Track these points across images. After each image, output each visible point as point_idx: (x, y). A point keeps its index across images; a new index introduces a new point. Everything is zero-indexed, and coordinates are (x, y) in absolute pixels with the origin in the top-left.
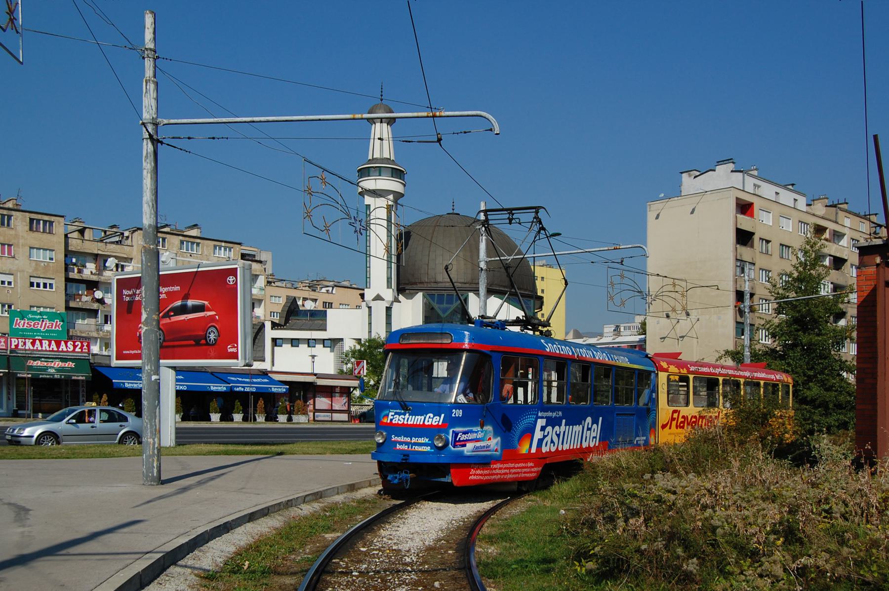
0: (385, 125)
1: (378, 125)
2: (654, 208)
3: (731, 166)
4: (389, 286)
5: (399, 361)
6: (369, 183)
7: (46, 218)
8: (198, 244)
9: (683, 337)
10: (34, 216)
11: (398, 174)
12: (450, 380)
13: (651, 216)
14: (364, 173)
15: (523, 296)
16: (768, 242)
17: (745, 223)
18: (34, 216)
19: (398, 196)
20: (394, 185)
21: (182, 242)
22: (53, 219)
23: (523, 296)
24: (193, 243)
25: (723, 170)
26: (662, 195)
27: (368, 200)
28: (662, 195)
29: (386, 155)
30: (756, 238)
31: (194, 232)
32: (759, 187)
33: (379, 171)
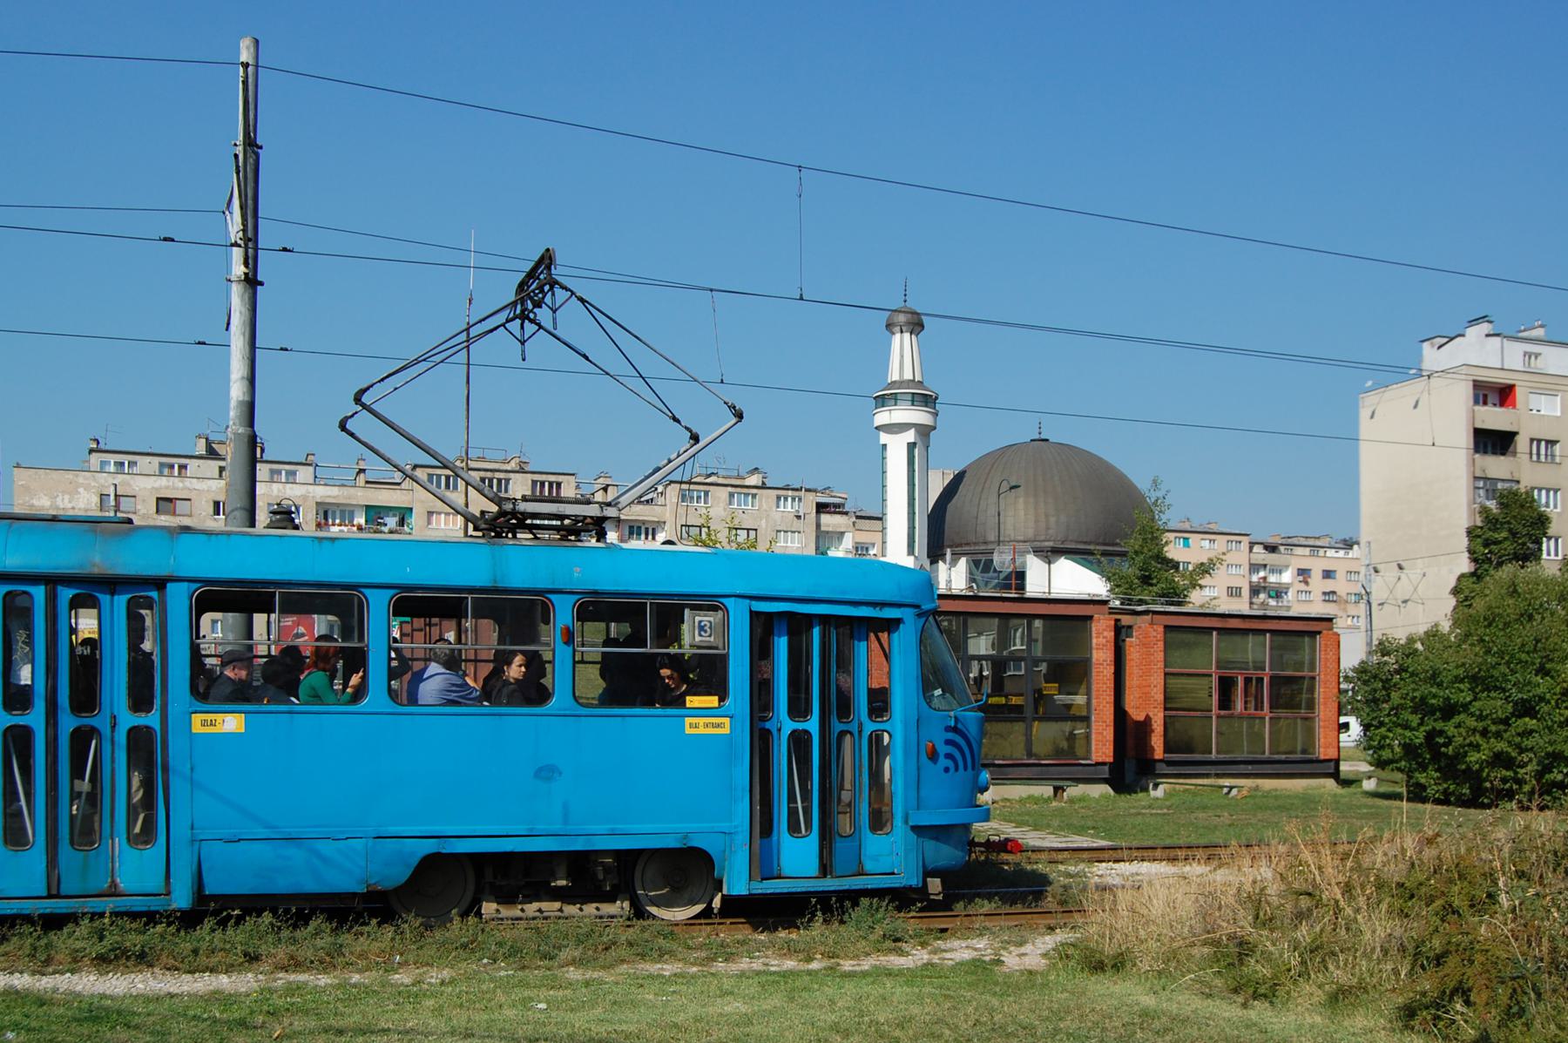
0: (907, 336)
1: (898, 336)
2: (1368, 402)
3: (1485, 328)
4: (911, 551)
5: (459, 625)
6: (883, 417)
7: (553, 478)
8: (754, 496)
9: (1405, 602)
10: (536, 477)
11: (927, 401)
12: (608, 642)
13: (1364, 414)
14: (882, 401)
15: (1104, 554)
16: (1551, 443)
17: (1495, 418)
18: (536, 477)
19: (924, 431)
20: (920, 416)
21: (731, 495)
22: (560, 479)
23: (1104, 554)
24: (747, 495)
25: (1476, 332)
26: (1370, 383)
27: (884, 438)
28: (1370, 383)
29: (908, 376)
30: (1522, 443)
31: (754, 480)
32: (1537, 355)
33: (895, 399)
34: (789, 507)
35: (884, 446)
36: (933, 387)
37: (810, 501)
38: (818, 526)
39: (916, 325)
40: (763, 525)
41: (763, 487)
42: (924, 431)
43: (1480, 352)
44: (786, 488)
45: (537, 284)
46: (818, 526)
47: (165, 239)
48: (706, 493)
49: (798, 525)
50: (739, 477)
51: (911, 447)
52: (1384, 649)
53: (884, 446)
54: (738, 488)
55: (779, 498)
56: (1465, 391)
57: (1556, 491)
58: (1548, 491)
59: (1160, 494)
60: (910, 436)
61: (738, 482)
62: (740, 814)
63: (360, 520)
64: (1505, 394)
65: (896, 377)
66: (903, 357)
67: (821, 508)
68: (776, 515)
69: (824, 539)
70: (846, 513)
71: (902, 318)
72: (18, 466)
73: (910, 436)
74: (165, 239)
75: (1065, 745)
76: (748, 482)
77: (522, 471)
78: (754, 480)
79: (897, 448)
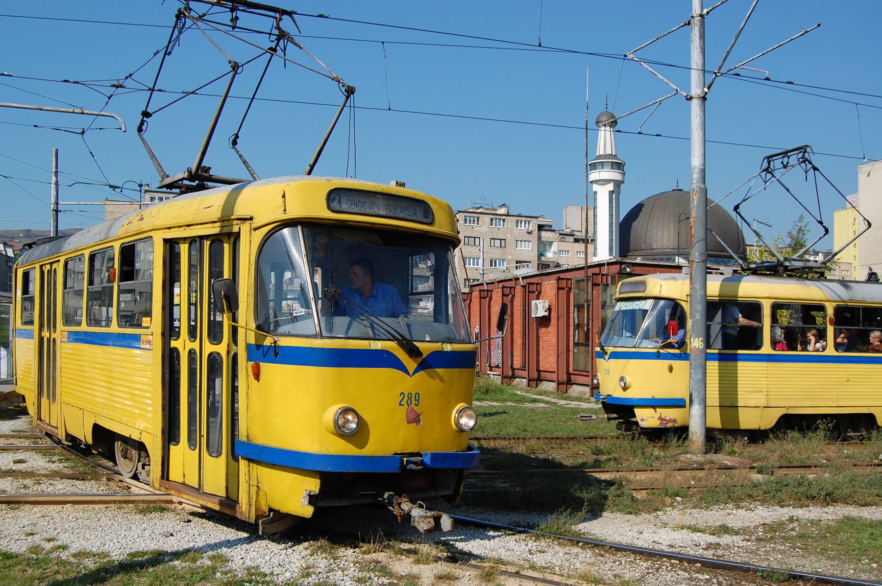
0: (608, 128)
4: (611, 254)
6: (594, 176)
11: (619, 166)
14: (594, 166)
19: (618, 184)
20: (615, 175)
24: (500, 220)
27: (595, 187)
29: (609, 152)
34: (523, 227)
35: (596, 192)
36: (622, 158)
37: (533, 226)
38: (539, 238)
40: (509, 237)
41: (508, 215)
42: (618, 184)
44: (519, 216)
45: (819, 25)
46: (539, 238)
47: (65, 81)
48: (478, 218)
49: (529, 237)
50: (493, 209)
51: (611, 193)
53: (596, 192)
54: (495, 217)
55: (517, 221)
57: (503, 261)
58: (474, 259)
59: (803, 224)
61: (493, 212)
62: (34, 387)
65: (602, 153)
66: (605, 141)
67: (541, 228)
68: (516, 231)
69: (543, 246)
70: (554, 231)
73: (611, 187)
74: (65, 81)
76: (498, 212)
78: (503, 211)
79: (603, 194)
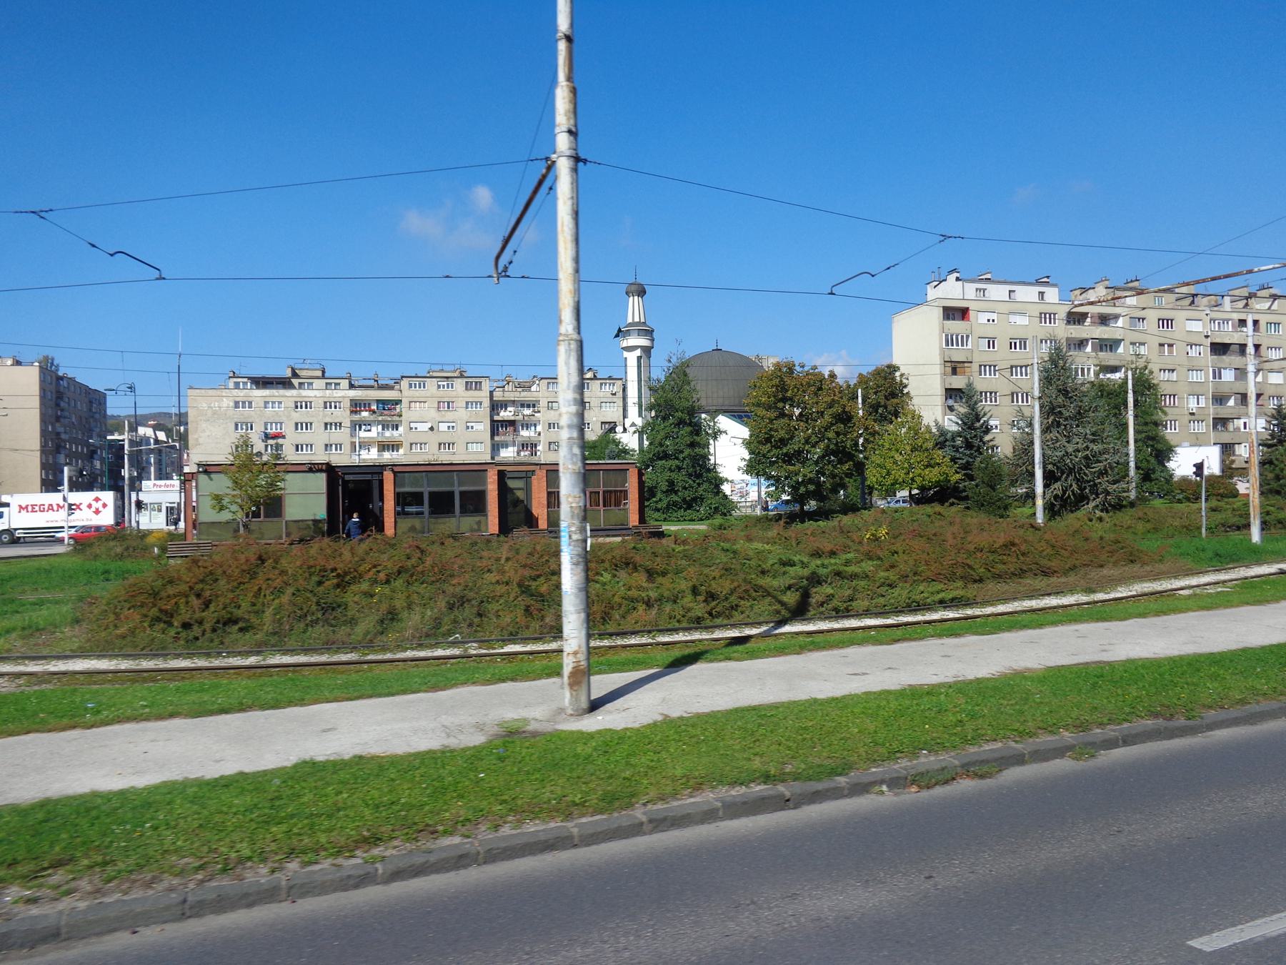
3: (956, 275)
11: (649, 333)
19: (647, 351)
20: (644, 342)
27: (626, 354)
29: (637, 320)
33: (628, 333)
34: (607, 389)
36: (651, 324)
39: (641, 292)
42: (647, 351)
43: (952, 291)
51: (639, 358)
52: (1263, 444)
56: (939, 313)
57: (1171, 346)
60: (638, 353)
63: (374, 407)
64: (963, 313)
66: (634, 309)
71: (633, 288)
72: (191, 388)
73: (638, 353)
75: (476, 527)
77: (462, 376)
